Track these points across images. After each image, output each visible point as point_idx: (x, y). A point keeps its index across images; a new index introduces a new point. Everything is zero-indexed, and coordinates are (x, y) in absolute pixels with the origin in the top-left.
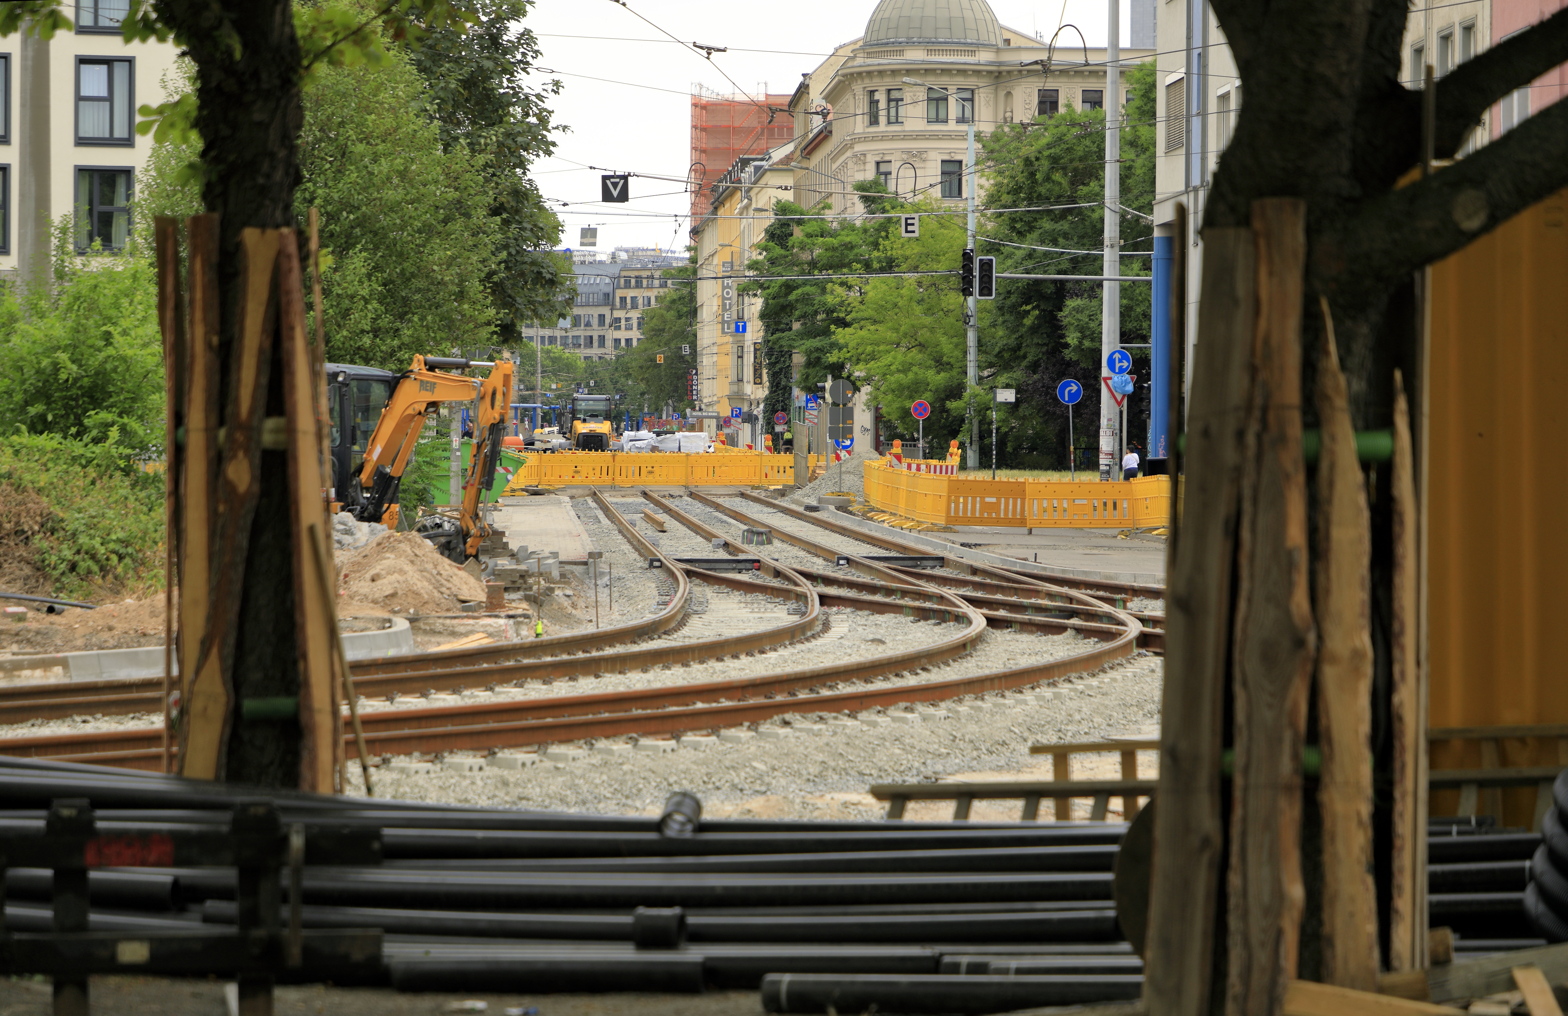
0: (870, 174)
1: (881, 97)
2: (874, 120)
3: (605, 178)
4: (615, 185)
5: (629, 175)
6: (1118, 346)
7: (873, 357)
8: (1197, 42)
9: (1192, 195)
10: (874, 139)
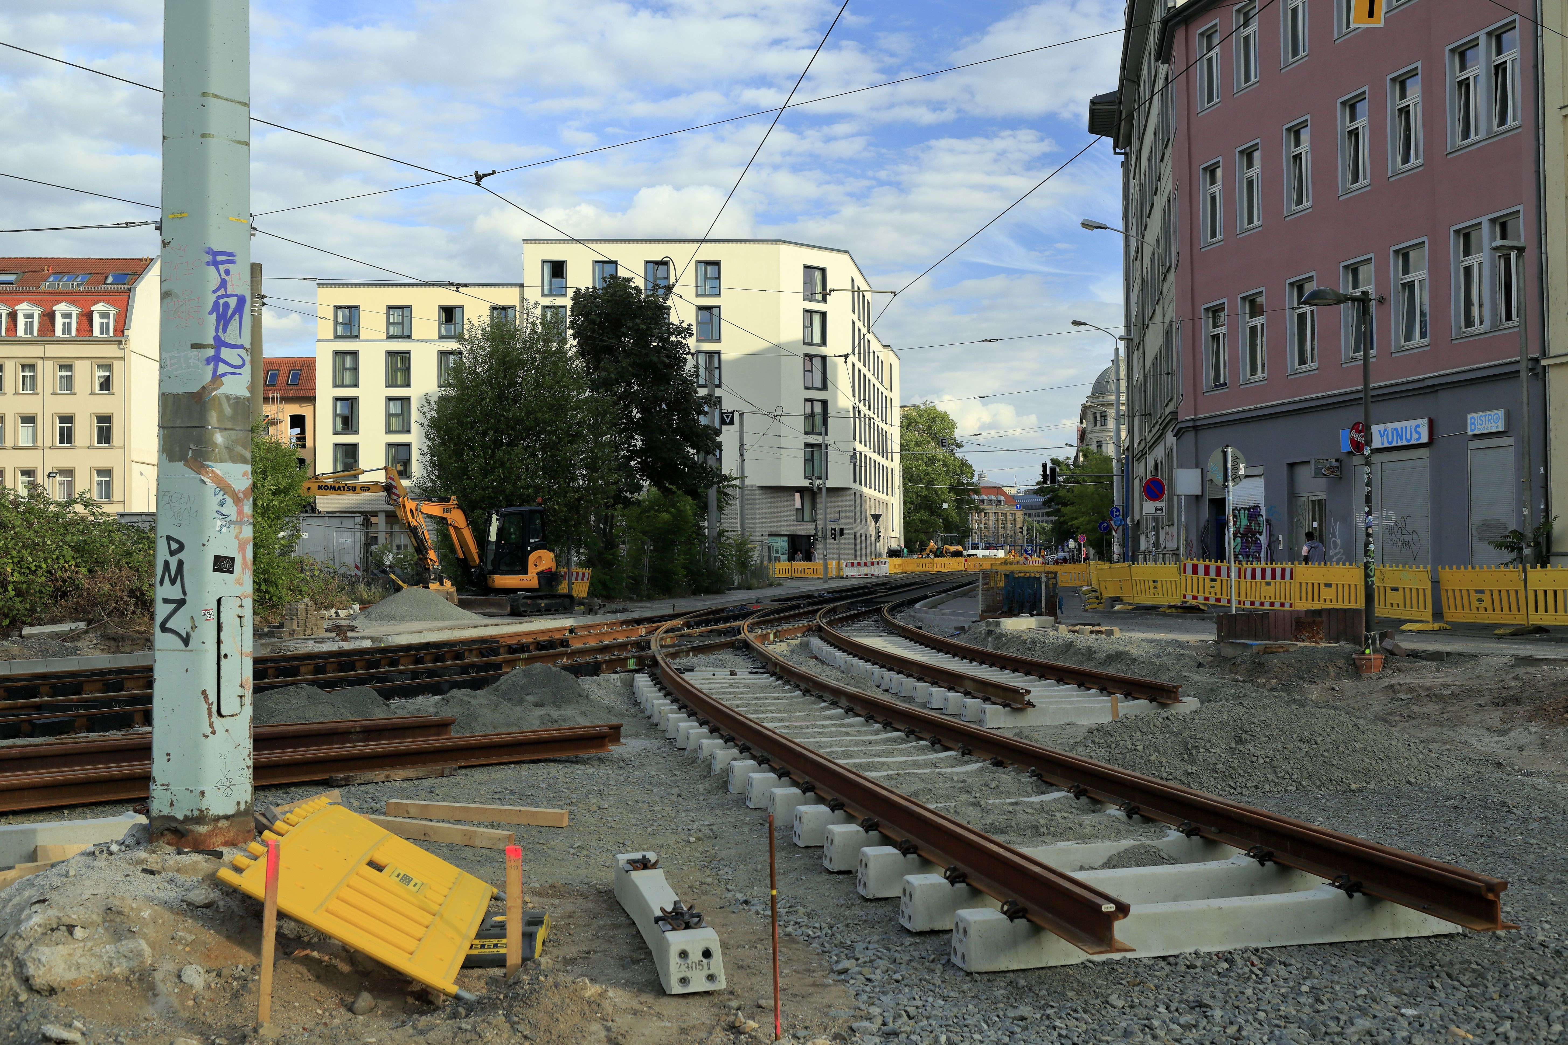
2: (1095, 425)
7: (1076, 519)
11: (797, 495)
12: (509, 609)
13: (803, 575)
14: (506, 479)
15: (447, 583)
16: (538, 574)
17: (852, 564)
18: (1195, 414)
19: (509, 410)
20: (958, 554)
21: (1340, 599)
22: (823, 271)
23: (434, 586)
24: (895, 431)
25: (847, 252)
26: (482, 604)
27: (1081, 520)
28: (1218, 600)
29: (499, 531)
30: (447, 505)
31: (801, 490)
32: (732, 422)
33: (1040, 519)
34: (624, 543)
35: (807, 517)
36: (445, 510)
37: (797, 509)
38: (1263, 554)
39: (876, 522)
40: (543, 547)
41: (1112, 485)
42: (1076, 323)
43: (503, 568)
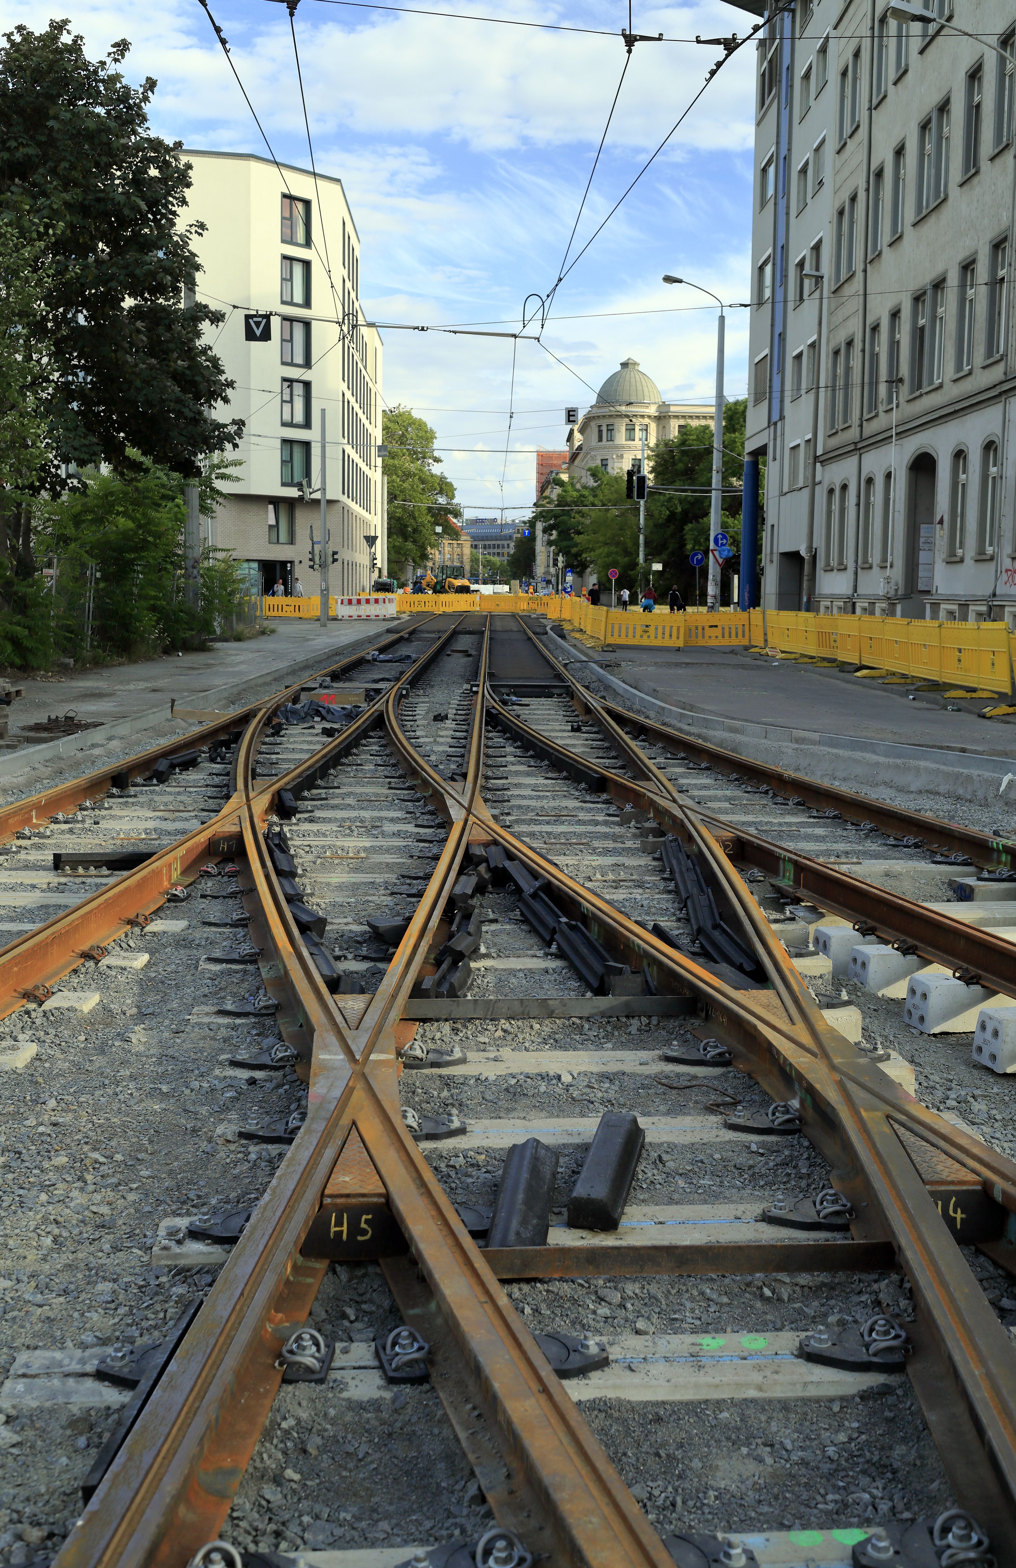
1: (604, 429)
2: (600, 439)
3: (248, 317)
4: (258, 324)
5: (271, 314)
6: (720, 531)
7: (593, 550)
9: (772, 428)
11: (271, 507)
13: (280, 614)
17: (350, 602)
20: (465, 590)
21: (660, 635)
22: (307, 203)
24: (377, 435)
25: (338, 181)
27: (598, 551)
31: (275, 501)
32: (266, 336)
34: (49, 565)
35: (283, 536)
37: (270, 526)
39: (371, 547)
41: (638, 509)
42: (669, 279)
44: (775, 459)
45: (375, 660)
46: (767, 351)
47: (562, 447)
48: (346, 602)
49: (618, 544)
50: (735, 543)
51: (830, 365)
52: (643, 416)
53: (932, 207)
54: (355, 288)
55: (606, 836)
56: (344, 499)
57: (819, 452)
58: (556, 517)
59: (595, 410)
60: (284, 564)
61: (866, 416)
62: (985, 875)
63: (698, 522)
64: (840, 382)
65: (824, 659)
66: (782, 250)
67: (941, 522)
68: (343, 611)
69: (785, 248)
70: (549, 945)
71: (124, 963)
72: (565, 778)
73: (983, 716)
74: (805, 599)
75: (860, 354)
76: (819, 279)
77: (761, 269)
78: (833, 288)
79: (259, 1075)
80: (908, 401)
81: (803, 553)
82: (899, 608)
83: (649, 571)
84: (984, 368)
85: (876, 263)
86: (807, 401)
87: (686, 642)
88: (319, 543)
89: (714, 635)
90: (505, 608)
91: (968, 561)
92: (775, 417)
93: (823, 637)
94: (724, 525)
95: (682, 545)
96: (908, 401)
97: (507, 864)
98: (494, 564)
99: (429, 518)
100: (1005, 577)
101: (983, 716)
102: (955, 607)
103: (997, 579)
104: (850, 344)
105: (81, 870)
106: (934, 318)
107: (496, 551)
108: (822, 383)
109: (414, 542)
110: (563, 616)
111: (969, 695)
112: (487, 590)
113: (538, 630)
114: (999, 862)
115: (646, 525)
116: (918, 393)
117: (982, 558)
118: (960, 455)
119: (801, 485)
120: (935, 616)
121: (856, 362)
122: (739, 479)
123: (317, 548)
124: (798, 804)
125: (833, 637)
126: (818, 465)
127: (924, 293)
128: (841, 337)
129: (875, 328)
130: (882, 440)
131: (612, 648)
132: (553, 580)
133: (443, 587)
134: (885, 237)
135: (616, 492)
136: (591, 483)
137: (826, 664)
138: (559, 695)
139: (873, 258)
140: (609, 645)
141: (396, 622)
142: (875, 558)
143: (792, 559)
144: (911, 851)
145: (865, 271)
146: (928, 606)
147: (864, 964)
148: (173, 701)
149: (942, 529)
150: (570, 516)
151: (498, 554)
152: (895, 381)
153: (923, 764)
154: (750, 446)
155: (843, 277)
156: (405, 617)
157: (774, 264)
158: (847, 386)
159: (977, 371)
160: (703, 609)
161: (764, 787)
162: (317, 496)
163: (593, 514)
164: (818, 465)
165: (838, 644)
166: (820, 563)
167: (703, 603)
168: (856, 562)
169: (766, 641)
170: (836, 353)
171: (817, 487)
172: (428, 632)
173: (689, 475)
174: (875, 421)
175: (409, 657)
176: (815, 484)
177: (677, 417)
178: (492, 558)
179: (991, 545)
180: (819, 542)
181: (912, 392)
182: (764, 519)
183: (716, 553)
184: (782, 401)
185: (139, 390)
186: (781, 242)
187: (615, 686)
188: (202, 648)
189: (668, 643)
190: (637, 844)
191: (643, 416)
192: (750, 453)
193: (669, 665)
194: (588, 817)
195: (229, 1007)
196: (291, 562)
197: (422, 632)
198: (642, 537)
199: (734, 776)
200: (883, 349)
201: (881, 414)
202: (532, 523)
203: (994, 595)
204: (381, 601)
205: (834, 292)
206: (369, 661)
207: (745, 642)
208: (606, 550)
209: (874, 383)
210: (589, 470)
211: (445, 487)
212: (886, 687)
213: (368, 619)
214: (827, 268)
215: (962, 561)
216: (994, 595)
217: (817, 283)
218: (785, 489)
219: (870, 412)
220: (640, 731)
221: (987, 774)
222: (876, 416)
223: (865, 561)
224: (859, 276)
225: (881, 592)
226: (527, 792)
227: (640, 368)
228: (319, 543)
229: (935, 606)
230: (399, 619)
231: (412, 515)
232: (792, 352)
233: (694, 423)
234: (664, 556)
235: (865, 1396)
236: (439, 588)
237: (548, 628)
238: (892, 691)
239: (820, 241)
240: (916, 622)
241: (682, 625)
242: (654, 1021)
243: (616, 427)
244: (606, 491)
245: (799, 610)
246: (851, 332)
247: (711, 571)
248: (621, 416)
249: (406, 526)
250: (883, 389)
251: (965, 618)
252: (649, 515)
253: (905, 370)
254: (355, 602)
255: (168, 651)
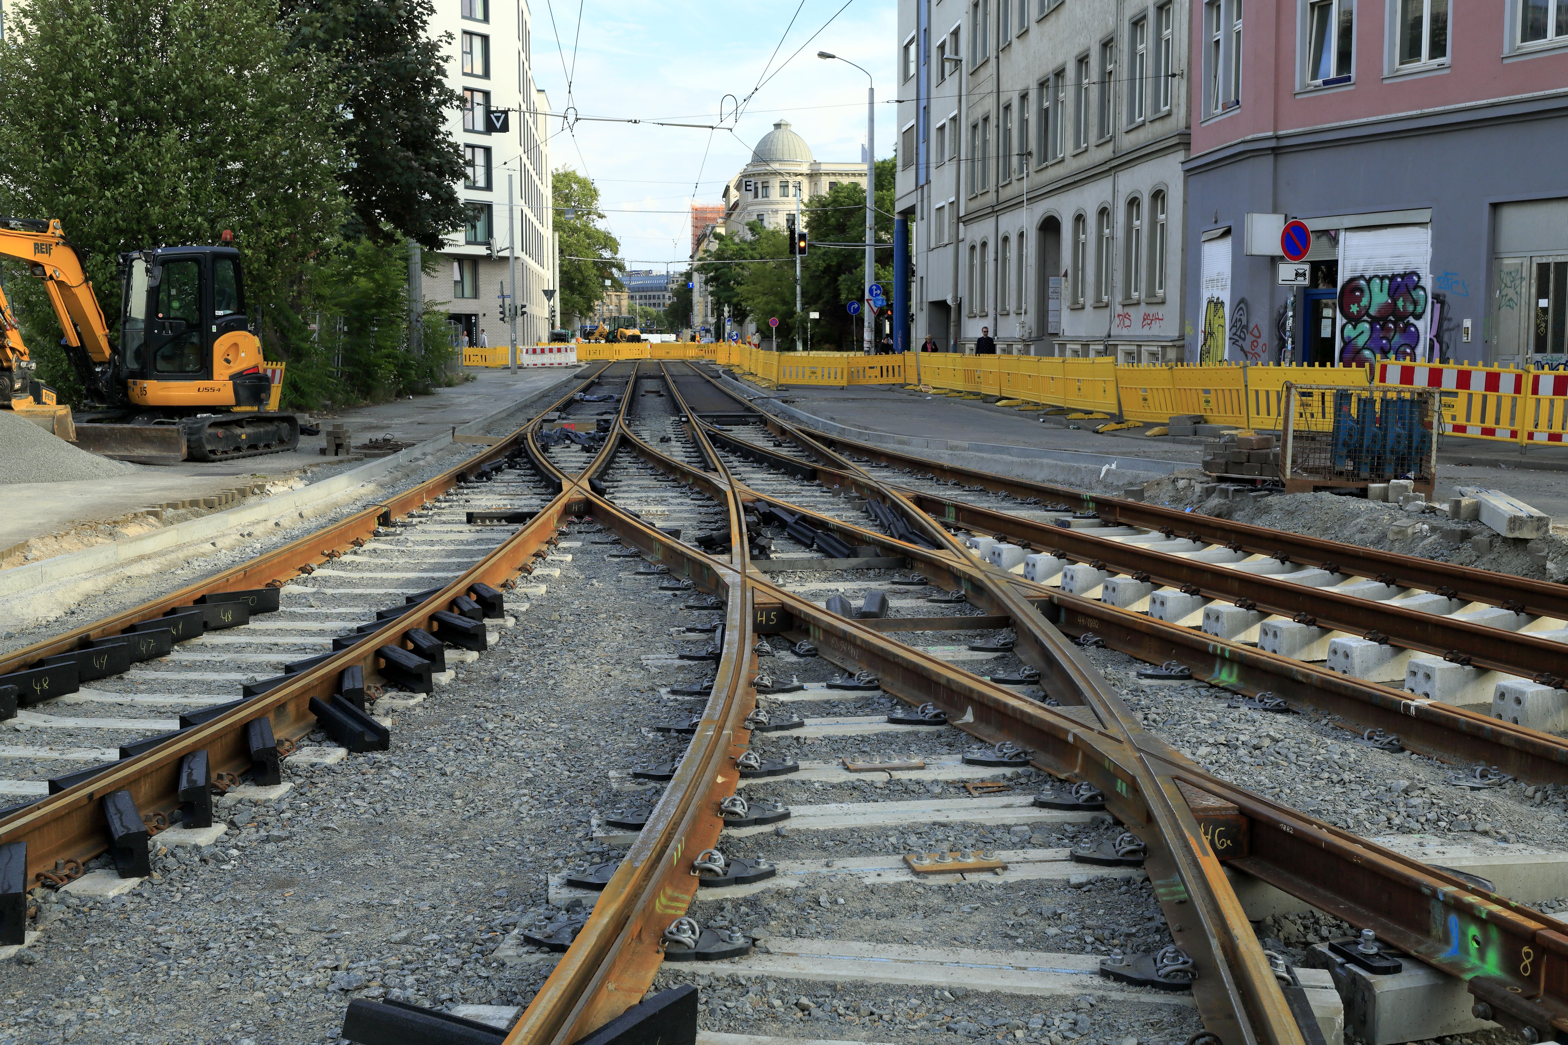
0: (755, 218)
1: (760, 186)
2: (756, 196)
4: (498, 118)
6: (874, 282)
8: (923, 95)
9: (919, 191)
10: (756, 204)
11: (456, 265)
12: (184, 450)
14: (151, 194)
15: (49, 396)
16: (232, 378)
17: (534, 351)
18: (1275, 130)
19: (149, 64)
20: (635, 339)
23: (22, 404)
26: (124, 439)
27: (757, 301)
28: (1461, 429)
29: (153, 293)
30: (42, 238)
32: (505, 128)
33: (643, 301)
35: (468, 291)
36: (38, 248)
37: (456, 282)
38: (1419, 350)
39: (549, 300)
40: (242, 326)
41: (795, 262)
42: (823, 55)
43: (161, 365)
44: (922, 219)
45: (582, 400)
46: (913, 122)
47: (719, 202)
48: (530, 351)
49: (776, 294)
50: (886, 293)
51: (969, 137)
52: (796, 175)
53: (1052, 8)
54: (528, 59)
55: (825, 503)
56: (522, 255)
57: (962, 214)
58: (717, 270)
59: (750, 168)
60: (468, 317)
61: (1001, 183)
62: (1078, 514)
63: (851, 273)
64: (978, 154)
65: (970, 393)
66: (924, 34)
67: (1066, 275)
68: (527, 359)
69: (927, 31)
70: (812, 546)
71: (561, 559)
72: (783, 474)
73: (1097, 432)
74: (952, 343)
75: (995, 129)
76: (958, 62)
77: (906, 48)
78: (971, 71)
79: (677, 592)
80: (1036, 172)
81: (950, 302)
82: (1032, 348)
83: (806, 319)
84: (1097, 146)
85: (1007, 50)
86: (949, 170)
87: (849, 381)
88: (509, 296)
89: (873, 375)
90: (676, 355)
91: (1088, 308)
92: (922, 181)
93: (969, 375)
94: (877, 277)
95: (837, 294)
96: (1036, 172)
97: (772, 509)
98: (650, 314)
99: (595, 271)
100: (1117, 321)
101: (1097, 432)
102: (1078, 347)
103: (1111, 323)
104: (986, 119)
105: (488, 522)
106: (1056, 101)
107: (652, 301)
108: (963, 157)
109: (581, 294)
110: (732, 362)
111: (1086, 417)
112: (655, 338)
113: (712, 374)
114: (1088, 508)
115: (802, 277)
116: (1044, 165)
117: (1099, 305)
118: (1079, 218)
119: (946, 241)
120: (1062, 353)
121: (992, 136)
122: (887, 232)
123: (508, 301)
124: (955, 484)
125: (977, 374)
126: (961, 224)
127: (1048, 80)
128: (978, 114)
129: (1007, 108)
130: (1015, 204)
131: (788, 388)
132: (712, 328)
133: (615, 337)
134: (1014, 30)
135: (774, 245)
136: (749, 237)
137: (972, 397)
138: (754, 423)
139: (1004, 47)
140: (781, 385)
141: (579, 370)
142: (1012, 306)
143: (940, 306)
144: (1032, 506)
145: (998, 57)
146: (1057, 347)
147: (999, 555)
148: (454, 429)
149: (1066, 281)
150: (730, 268)
151: (654, 304)
152: (1025, 154)
153: (1045, 461)
154: (900, 206)
155: (979, 62)
156: (585, 366)
157: (918, 45)
158: (984, 159)
159: (1092, 149)
160: (860, 354)
161: (930, 475)
162: (506, 253)
163: (751, 266)
164: (961, 224)
165: (981, 380)
166: (965, 311)
167: (861, 348)
168: (996, 309)
169: (919, 380)
170: (975, 127)
171: (961, 244)
172: (613, 377)
173: (841, 228)
174: (1009, 188)
175: (611, 397)
176: (958, 241)
177: (828, 174)
178: (648, 309)
179: (1106, 294)
180: (963, 292)
181: (1039, 164)
182: (913, 272)
183: (871, 303)
184: (928, 168)
185: (401, 175)
186: (924, 26)
187: (797, 416)
188: (425, 392)
189: (833, 382)
190: (849, 506)
191: (796, 175)
192: (900, 213)
193: (838, 400)
194: (809, 494)
195: (642, 570)
196: (476, 315)
197: (606, 377)
198: (798, 288)
199: (908, 470)
200: (1014, 125)
201: (1014, 182)
202: (688, 276)
203: (1109, 336)
204: (563, 350)
205: (972, 74)
206: (577, 401)
207: (901, 380)
208: (765, 299)
209: (1007, 156)
210: (748, 224)
211: (609, 242)
212: (1022, 413)
213: (551, 367)
214: (964, 53)
215: (1083, 308)
216: (1109, 336)
217: (956, 65)
218: (933, 245)
219: (1005, 179)
220: (830, 443)
221: (1091, 466)
222: (1010, 183)
223: (1004, 309)
224: (993, 61)
225: (1017, 335)
226: (760, 482)
227: (792, 129)
228: (509, 296)
229: (1063, 346)
230: (580, 366)
231: (579, 269)
232: (935, 124)
233: (845, 181)
234: (820, 305)
235: (995, 659)
236: (611, 338)
237: (720, 372)
238: (1026, 416)
239: (959, 28)
240: (1046, 359)
241: (845, 366)
242: (883, 571)
243: (770, 184)
244: (765, 245)
245: (947, 351)
246: (987, 110)
247: (866, 319)
248: (776, 173)
249: (573, 279)
250: (1015, 160)
251: (1086, 355)
252: (805, 267)
253: (1033, 145)
254: (538, 351)
255: (400, 395)
